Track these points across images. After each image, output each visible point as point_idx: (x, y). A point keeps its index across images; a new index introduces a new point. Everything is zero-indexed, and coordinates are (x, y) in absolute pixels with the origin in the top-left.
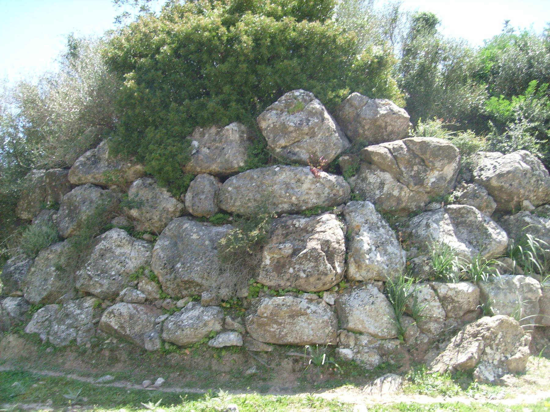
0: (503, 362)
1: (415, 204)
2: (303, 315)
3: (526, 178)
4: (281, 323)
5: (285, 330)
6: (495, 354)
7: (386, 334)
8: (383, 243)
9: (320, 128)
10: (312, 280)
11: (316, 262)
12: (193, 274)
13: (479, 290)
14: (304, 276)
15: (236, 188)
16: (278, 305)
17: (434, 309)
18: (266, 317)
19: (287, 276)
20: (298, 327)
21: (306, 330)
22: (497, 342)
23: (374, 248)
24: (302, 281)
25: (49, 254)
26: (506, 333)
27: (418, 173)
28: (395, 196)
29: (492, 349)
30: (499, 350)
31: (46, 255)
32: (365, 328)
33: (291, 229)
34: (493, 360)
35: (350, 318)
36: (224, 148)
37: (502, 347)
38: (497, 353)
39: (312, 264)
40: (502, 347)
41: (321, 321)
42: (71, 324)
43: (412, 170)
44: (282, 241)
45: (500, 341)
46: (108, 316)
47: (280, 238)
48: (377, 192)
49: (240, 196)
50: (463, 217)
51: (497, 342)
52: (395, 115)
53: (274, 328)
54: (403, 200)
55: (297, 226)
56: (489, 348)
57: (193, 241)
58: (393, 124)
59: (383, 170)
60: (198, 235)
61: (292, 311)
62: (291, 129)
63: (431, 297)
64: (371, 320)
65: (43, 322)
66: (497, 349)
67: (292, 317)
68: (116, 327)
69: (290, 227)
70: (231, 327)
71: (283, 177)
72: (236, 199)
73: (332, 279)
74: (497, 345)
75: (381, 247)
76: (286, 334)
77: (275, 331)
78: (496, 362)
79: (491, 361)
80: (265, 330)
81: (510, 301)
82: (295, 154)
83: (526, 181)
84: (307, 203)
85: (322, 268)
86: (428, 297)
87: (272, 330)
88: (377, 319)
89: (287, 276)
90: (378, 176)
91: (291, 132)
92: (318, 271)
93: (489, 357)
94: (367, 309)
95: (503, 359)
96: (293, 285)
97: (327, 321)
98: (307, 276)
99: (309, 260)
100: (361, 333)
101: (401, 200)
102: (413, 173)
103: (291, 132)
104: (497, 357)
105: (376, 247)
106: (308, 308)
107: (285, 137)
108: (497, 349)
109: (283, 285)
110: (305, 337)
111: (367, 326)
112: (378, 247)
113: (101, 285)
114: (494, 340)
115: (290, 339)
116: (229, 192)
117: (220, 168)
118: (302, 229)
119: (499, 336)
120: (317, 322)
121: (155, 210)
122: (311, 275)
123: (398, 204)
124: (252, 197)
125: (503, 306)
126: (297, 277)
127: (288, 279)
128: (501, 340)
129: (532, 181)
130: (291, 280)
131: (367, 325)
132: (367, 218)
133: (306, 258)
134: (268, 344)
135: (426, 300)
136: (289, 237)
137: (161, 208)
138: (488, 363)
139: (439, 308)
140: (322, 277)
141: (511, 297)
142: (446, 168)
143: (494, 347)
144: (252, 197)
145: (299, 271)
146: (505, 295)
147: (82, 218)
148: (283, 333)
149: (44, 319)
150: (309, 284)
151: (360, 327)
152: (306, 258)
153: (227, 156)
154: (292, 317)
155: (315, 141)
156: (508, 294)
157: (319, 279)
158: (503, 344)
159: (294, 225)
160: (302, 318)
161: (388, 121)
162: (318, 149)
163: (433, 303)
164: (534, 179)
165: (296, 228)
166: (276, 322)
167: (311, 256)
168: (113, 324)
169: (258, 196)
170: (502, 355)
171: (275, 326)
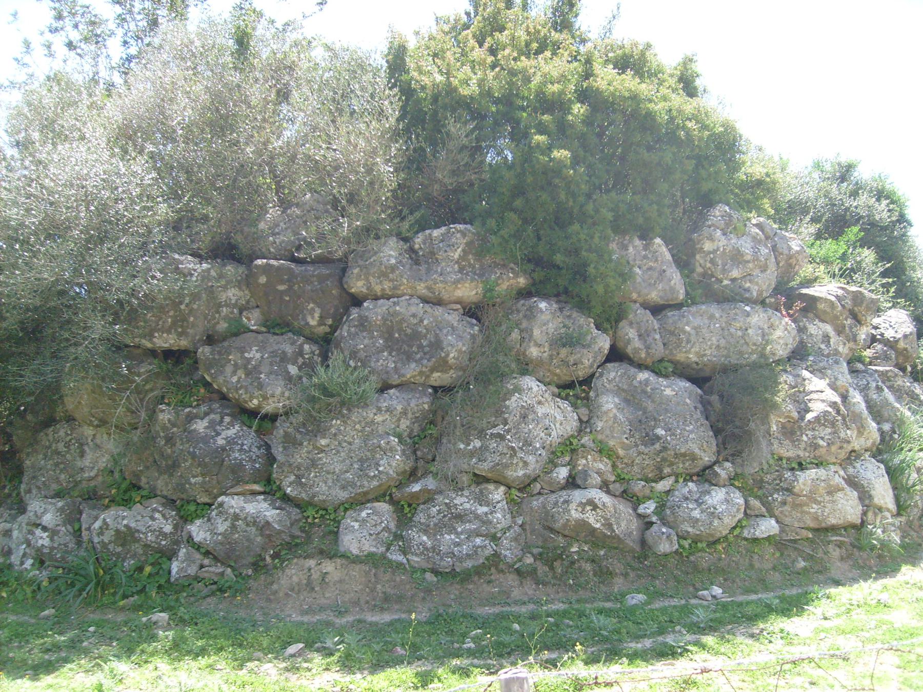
10: (833, 449)
11: (833, 427)
12: (690, 444)
14: (825, 444)
15: (695, 328)
19: (803, 446)
24: (823, 451)
25: (375, 414)
31: (371, 415)
35: (873, 493)
36: (664, 271)
39: (829, 430)
42: (475, 529)
46: (580, 509)
49: (701, 340)
50: (890, 381)
53: (814, 508)
57: (669, 399)
59: (823, 321)
60: (673, 390)
62: (748, 258)
65: (379, 533)
67: (830, 493)
68: (598, 526)
70: (757, 512)
72: (694, 343)
80: (802, 512)
84: (774, 354)
89: (803, 446)
91: (748, 262)
92: (839, 438)
96: (812, 456)
99: (824, 425)
103: (748, 262)
107: (738, 267)
113: (526, 464)
115: (833, 521)
116: (685, 332)
117: (661, 297)
121: (585, 351)
122: (833, 443)
124: (715, 342)
126: (816, 447)
127: (805, 449)
130: (808, 449)
133: (819, 423)
134: (808, 529)
137: (597, 349)
140: (845, 446)
144: (715, 342)
145: (815, 438)
147: (448, 355)
149: (379, 528)
152: (819, 423)
153: (673, 282)
157: (841, 448)
166: (816, 502)
167: (826, 420)
168: (591, 521)
169: (723, 342)
171: (814, 506)
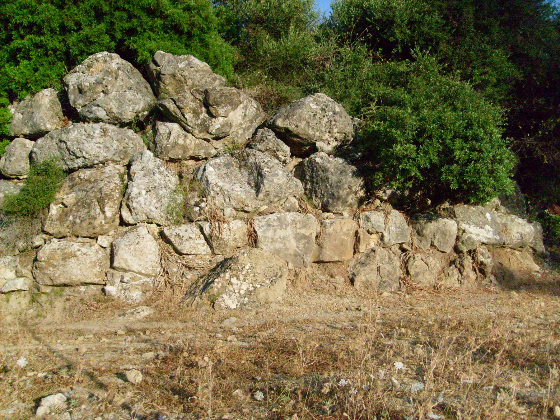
0: (251, 292)
1: (203, 151)
2: (73, 257)
3: (315, 119)
4: (56, 266)
5: (58, 272)
6: (241, 284)
7: (151, 272)
8: (155, 188)
9: (113, 86)
10: (85, 224)
11: (89, 208)
13: (122, 209)
16: (55, 249)
17: (199, 246)
18: (44, 261)
20: (68, 268)
21: (75, 270)
22: (244, 272)
23: (144, 192)
26: (256, 264)
27: (204, 120)
28: (180, 145)
29: (238, 279)
30: (247, 281)
32: (129, 266)
33: (76, 181)
34: (240, 290)
37: (250, 278)
38: (245, 283)
40: (250, 278)
41: (88, 261)
43: (199, 118)
44: (68, 191)
45: (247, 271)
47: (67, 190)
48: (165, 142)
51: (244, 272)
52: (193, 69)
54: (189, 147)
55: (81, 178)
56: (235, 278)
58: (192, 77)
61: (65, 254)
63: (196, 235)
64: (135, 259)
66: (244, 280)
69: (75, 179)
71: (75, 133)
73: (101, 223)
74: (245, 275)
75: (152, 191)
76: (59, 275)
77: (51, 274)
78: (242, 292)
79: (237, 291)
81: (280, 238)
82: (91, 113)
83: (315, 122)
85: (92, 213)
86: (193, 236)
87: (49, 272)
88: (142, 258)
90: (167, 127)
93: (234, 287)
94: (132, 249)
95: (251, 289)
97: (94, 262)
98: (81, 221)
100: (125, 271)
101: (187, 148)
102: (199, 122)
104: (244, 287)
105: (147, 192)
106: (79, 250)
108: (244, 280)
109: (63, 231)
110: (74, 277)
111: (130, 265)
112: (150, 191)
114: (242, 271)
118: (86, 180)
119: (247, 267)
120: (84, 263)
122: (84, 220)
123: (185, 152)
125: (271, 242)
127: (68, 226)
128: (249, 270)
129: (323, 122)
131: (130, 263)
132: (143, 165)
135: (190, 238)
136: (75, 189)
138: (234, 292)
139: (204, 245)
141: (281, 233)
142: (231, 114)
143: (242, 277)
146: (275, 231)
148: (57, 275)
150: (83, 229)
151: (124, 265)
154: (64, 259)
155: (109, 98)
156: (279, 230)
158: (252, 275)
159: (79, 177)
160: (73, 260)
161: (187, 74)
162: (113, 106)
163: (198, 241)
164: (326, 120)
165: (81, 179)
170: (251, 285)
171: (51, 269)
